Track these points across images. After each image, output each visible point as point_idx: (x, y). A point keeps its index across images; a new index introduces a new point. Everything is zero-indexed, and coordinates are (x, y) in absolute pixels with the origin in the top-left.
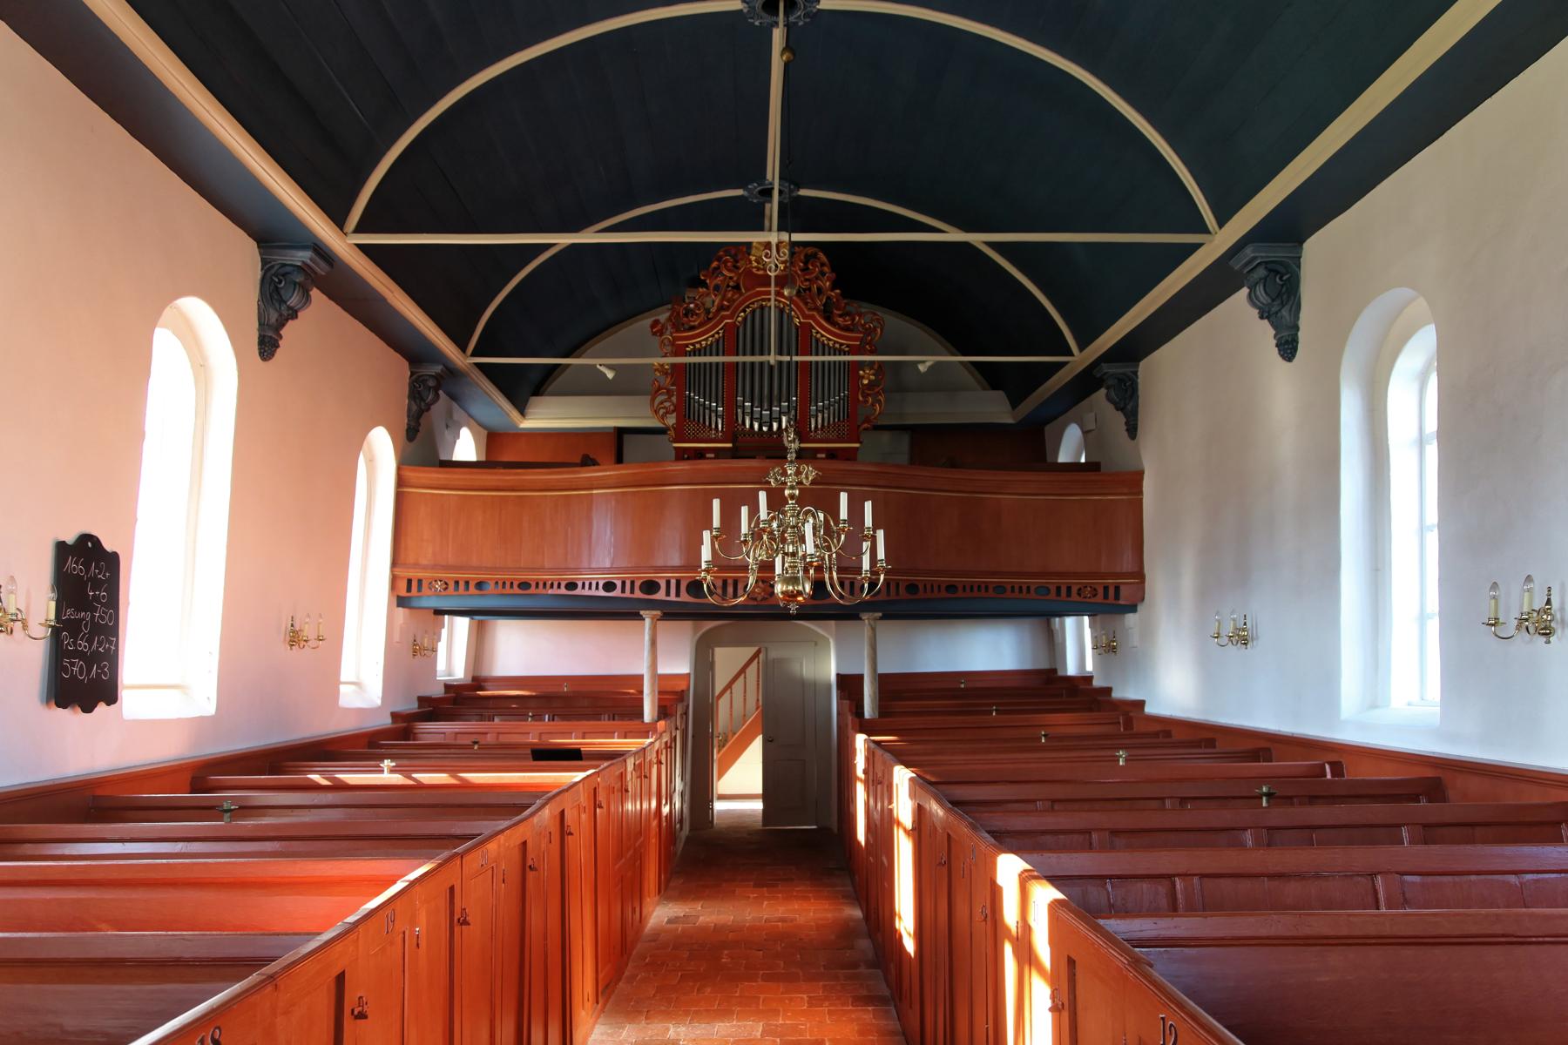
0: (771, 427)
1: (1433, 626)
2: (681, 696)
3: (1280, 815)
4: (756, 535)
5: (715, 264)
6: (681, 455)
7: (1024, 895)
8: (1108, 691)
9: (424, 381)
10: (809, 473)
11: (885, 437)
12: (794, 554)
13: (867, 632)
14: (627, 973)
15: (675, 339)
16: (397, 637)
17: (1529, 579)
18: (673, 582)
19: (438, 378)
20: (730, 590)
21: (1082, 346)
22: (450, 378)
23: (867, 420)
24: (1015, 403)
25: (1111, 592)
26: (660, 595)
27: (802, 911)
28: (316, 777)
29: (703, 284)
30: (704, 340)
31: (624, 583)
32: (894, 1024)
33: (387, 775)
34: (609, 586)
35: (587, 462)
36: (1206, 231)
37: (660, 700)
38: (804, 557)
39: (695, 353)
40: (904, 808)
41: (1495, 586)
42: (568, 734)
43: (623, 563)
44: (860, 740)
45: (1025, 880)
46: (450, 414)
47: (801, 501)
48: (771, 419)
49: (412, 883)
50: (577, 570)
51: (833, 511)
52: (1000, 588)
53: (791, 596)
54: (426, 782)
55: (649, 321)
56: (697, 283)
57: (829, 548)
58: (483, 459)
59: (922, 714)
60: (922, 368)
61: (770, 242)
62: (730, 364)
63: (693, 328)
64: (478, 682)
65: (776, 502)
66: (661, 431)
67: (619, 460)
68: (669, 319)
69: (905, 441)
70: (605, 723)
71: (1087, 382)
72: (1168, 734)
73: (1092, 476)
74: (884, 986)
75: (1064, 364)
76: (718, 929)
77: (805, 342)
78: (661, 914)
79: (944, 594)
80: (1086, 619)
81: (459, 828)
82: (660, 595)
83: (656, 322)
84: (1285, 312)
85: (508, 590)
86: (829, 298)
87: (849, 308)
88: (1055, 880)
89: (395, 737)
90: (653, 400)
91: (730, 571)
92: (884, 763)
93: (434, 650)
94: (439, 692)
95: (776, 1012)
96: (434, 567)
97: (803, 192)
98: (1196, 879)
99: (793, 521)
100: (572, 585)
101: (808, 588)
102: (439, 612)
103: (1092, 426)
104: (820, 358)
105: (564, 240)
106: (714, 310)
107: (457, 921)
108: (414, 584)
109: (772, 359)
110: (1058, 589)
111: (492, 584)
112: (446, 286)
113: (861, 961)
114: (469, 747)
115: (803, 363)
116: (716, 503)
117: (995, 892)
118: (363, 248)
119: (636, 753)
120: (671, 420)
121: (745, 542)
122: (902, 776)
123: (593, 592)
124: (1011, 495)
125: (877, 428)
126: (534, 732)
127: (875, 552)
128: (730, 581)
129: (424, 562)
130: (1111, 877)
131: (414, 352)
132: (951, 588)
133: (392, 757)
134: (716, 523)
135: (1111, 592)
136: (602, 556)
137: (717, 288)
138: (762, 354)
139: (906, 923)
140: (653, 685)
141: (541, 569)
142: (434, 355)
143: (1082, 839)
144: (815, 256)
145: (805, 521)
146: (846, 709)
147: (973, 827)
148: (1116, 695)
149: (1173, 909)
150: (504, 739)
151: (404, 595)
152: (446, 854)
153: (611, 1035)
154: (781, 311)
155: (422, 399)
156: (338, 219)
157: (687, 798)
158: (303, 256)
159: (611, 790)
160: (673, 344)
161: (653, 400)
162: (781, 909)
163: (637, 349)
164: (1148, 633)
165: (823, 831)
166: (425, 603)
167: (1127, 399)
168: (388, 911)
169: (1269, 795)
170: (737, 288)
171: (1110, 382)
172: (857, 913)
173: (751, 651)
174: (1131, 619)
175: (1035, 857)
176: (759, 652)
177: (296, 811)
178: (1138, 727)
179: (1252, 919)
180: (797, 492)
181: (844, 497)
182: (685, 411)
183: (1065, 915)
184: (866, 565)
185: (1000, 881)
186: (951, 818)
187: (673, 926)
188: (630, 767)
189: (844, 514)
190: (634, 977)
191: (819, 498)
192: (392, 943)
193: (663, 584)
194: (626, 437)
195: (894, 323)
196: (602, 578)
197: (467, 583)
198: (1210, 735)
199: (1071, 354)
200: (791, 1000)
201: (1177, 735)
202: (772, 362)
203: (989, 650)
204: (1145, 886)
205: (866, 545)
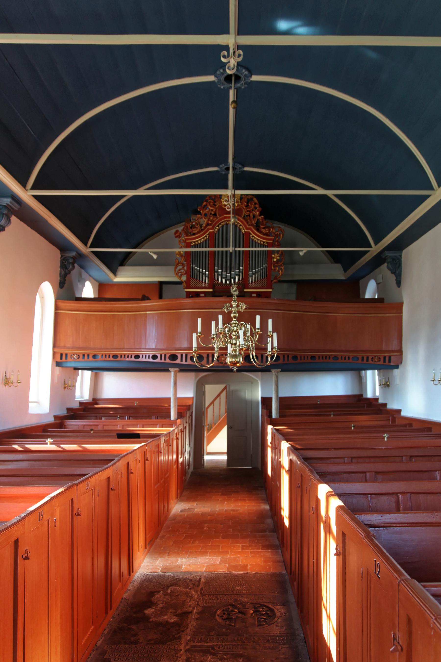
0: (231, 281)
2: (189, 408)
4: (218, 335)
5: (205, 203)
6: (189, 295)
7: (328, 502)
8: (385, 405)
9: (67, 260)
10: (243, 306)
11: (285, 286)
12: (235, 344)
13: (274, 378)
14: (160, 535)
15: (186, 239)
16: (56, 381)
18: (184, 355)
19: (74, 258)
20: (210, 359)
21: (376, 244)
22: (80, 257)
23: (276, 278)
25: (387, 359)
26: (178, 361)
27: (241, 506)
28: (16, 447)
29: (199, 213)
30: (200, 240)
31: (161, 356)
32: (280, 558)
33: (49, 445)
34: (155, 357)
35: (145, 298)
36: (432, 188)
37: (178, 409)
38: (239, 346)
39: (196, 246)
40: (285, 461)
42: (136, 426)
43: (160, 346)
44: (270, 428)
45: (328, 496)
46: (80, 275)
47: (239, 319)
48: (231, 278)
49: (52, 498)
50: (140, 349)
51: (253, 324)
52: (336, 358)
53: (234, 363)
54: (67, 449)
55: (174, 231)
56: (196, 212)
58: (97, 296)
59: (297, 413)
60: (301, 254)
61: (229, 195)
62: (211, 252)
63: (194, 234)
64: (95, 401)
65: (227, 320)
66: (180, 283)
67: (161, 297)
68: (183, 230)
69: (294, 288)
70: (153, 420)
71: (378, 261)
72: (411, 425)
73: (379, 305)
74: (277, 540)
75: (368, 251)
76: (203, 514)
77: (246, 241)
78: (177, 508)
79: (310, 360)
80: (376, 371)
81: (78, 471)
82: (178, 361)
83: (177, 231)
85: (107, 359)
86: (258, 220)
87: (268, 225)
88: (340, 496)
89: (56, 427)
90: (176, 268)
92: (278, 439)
93: (74, 386)
94: (77, 406)
95: (227, 552)
96: (73, 348)
97: (246, 169)
98: (408, 495)
99: (235, 329)
100: (137, 357)
101: (241, 359)
102: (76, 369)
103: (381, 281)
104: (254, 249)
105: (130, 193)
106: (204, 225)
107: (75, 514)
108: (64, 356)
109: (231, 249)
111: (100, 356)
112: (77, 215)
113: (267, 530)
114: (89, 432)
115: (246, 251)
116: (199, 320)
117: (318, 501)
118: (35, 197)
119: (165, 435)
120: (184, 278)
121: (213, 338)
122: (285, 445)
123: (147, 360)
124: (342, 314)
125: (280, 281)
126: (120, 425)
127: (272, 343)
128: (210, 355)
129: (68, 345)
130: (370, 494)
131: (63, 246)
132: (313, 357)
133: (51, 437)
135: (387, 359)
136: (151, 343)
137: (205, 215)
138: (227, 247)
139: (285, 513)
140: (175, 403)
141: (123, 349)
142: (72, 248)
144: (252, 199)
145: (240, 329)
146: (265, 414)
147: (311, 471)
149: (398, 510)
150: (106, 428)
151: (59, 361)
152: (69, 484)
153: (152, 563)
154: (236, 226)
155: (66, 268)
156: (23, 184)
157: (192, 454)
158: (7, 201)
159: (152, 452)
160: (185, 242)
161: (176, 268)
162: (232, 505)
163: (170, 244)
164: (403, 377)
165: (255, 469)
166: (69, 365)
167: (397, 268)
168: (40, 511)
170: (215, 215)
171: (389, 260)
172: (267, 507)
173: (223, 386)
174: (396, 372)
175: (333, 485)
176: (225, 388)
177: (6, 463)
178: (398, 422)
179: (425, 515)
180: (237, 315)
181: (258, 318)
182: (191, 274)
183: (343, 513)
184: (269, 349)
185: (319, 496)
186: (302, 466)
187: (181, 513)
189: (258, 325)
190: (164, 536)
191: (246, 317)
192: (42, 525)
195: (290, 232)
196: (152, 353)
197: (88, 355)
199: (370, 246)
200: (234, 547)
201: (415, 426)
202: (231, 251)
203: (332, 385)
204: (385, 498)
205: (269, 339)
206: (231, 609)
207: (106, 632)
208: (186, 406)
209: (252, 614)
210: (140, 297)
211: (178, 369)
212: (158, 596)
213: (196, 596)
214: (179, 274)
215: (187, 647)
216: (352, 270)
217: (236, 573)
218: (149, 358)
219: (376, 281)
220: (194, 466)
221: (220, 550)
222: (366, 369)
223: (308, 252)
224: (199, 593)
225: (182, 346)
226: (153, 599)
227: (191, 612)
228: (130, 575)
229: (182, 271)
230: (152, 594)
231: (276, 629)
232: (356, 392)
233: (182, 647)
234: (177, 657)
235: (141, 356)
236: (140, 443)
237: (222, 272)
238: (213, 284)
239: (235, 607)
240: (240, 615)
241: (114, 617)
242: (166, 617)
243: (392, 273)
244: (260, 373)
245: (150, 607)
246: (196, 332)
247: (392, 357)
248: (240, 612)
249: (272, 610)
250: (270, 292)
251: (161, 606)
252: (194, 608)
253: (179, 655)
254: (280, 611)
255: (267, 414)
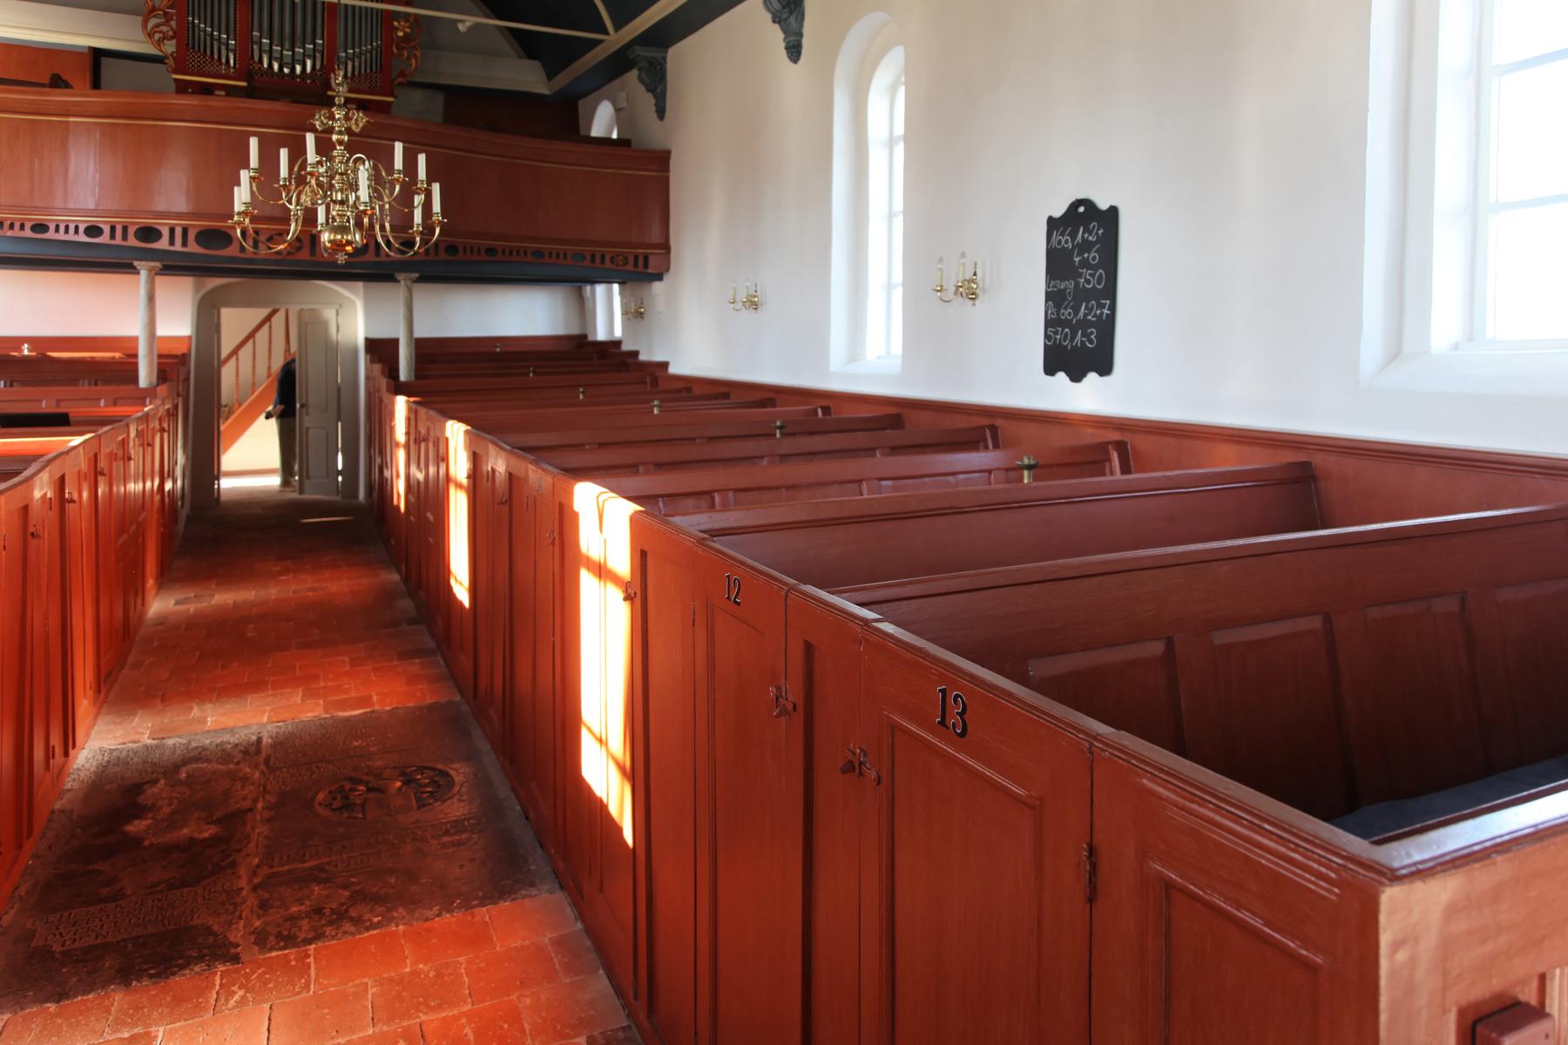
0: (293, 69)
1: (898, 294)
2: (183, 359)
3: (788, 445)
6: (182, 88)
8: (635, 354)
10: (360, 120)
11: (418, 95)
12: (342, 203)
14: (130, 660)
17: (963, 255)
18: (179, 231)
21: (618, 28)
23: (402, 74)
24: (551, 74)
26: (163, 244)
31: (113, 229)
34: (93, 231)
35: (57, 82)
38: (355, 206)
41: (941, 261)
47: (351, 148)
50: (47, 210)
52: (538, 253)
53: (338, 246)
57: (380, 198)
59: (454, 376)
65: (324, 148)
67: (96, 84)
69: (439, 99)
71: (619, 63)
72: (689, 390)
75: (600, 42)
78: (161, 605)
80: (616, 287)
82: (163, 244)
84: (792, 20)
91: (270, 218)
100: (40, 227)
110: (593, 256)
120: (170, 47)
123: (71, 237)
130: (662, 496)
132: (491, 251)
134: (254, 161)
143: (632, 468)
148: (643, 357)
159: (112, 457)
167: (656, 81)
169: (781, 428)
172: (396, 577)
174: (657, 286)
188: (133, 434)
189: (398, 163)
191: (369, 145)
193: (165, 232)
194: (105, 61)
196: (84, 222)
198: (725, 390)
203: (521, 314)
205: (418, 199)
206: (348, 786)
207: (22, 892)
208: (175, 357)
209: (400, 789)
210: (47, 81)
211: (158, 264)
212: (155, 790)
213: (257, 775)
214: (157, 36)
215: (256, 881)
216: (564, 79)
217: (347, 714)
218: (76, 231)
219: (614, 104)
220: (192, 502)
221: (298, 673)
222: (593, 282)
223: (477, 25)
224: (262, 767)
225: (173, 209)
226: (141, 799)
227: (251, 810)
228: (66, 754)
229: (164, 29)
230: (136, 788)
231: (456, 808)
232: (575, 331)
233: (243, 883)
234: (235, 905)
235: (52, 227)
236: (81, 434)
237: (271, 45)
238: (248, 69)
239: (360, 782)
240: (371, 795)
241: (35, 856)
242: (185, 831)
243: (648, 90)
244: (360, 285)
245: (137, 817)
246: (247, 166)
247: (651, 258)
248: (370, 790)
249: (445, 774)
250: (390, 103)
251: (167, 810)
252: (255, 801)
253: (238, 900)
254: (460, 772)
255: (383, 373)
